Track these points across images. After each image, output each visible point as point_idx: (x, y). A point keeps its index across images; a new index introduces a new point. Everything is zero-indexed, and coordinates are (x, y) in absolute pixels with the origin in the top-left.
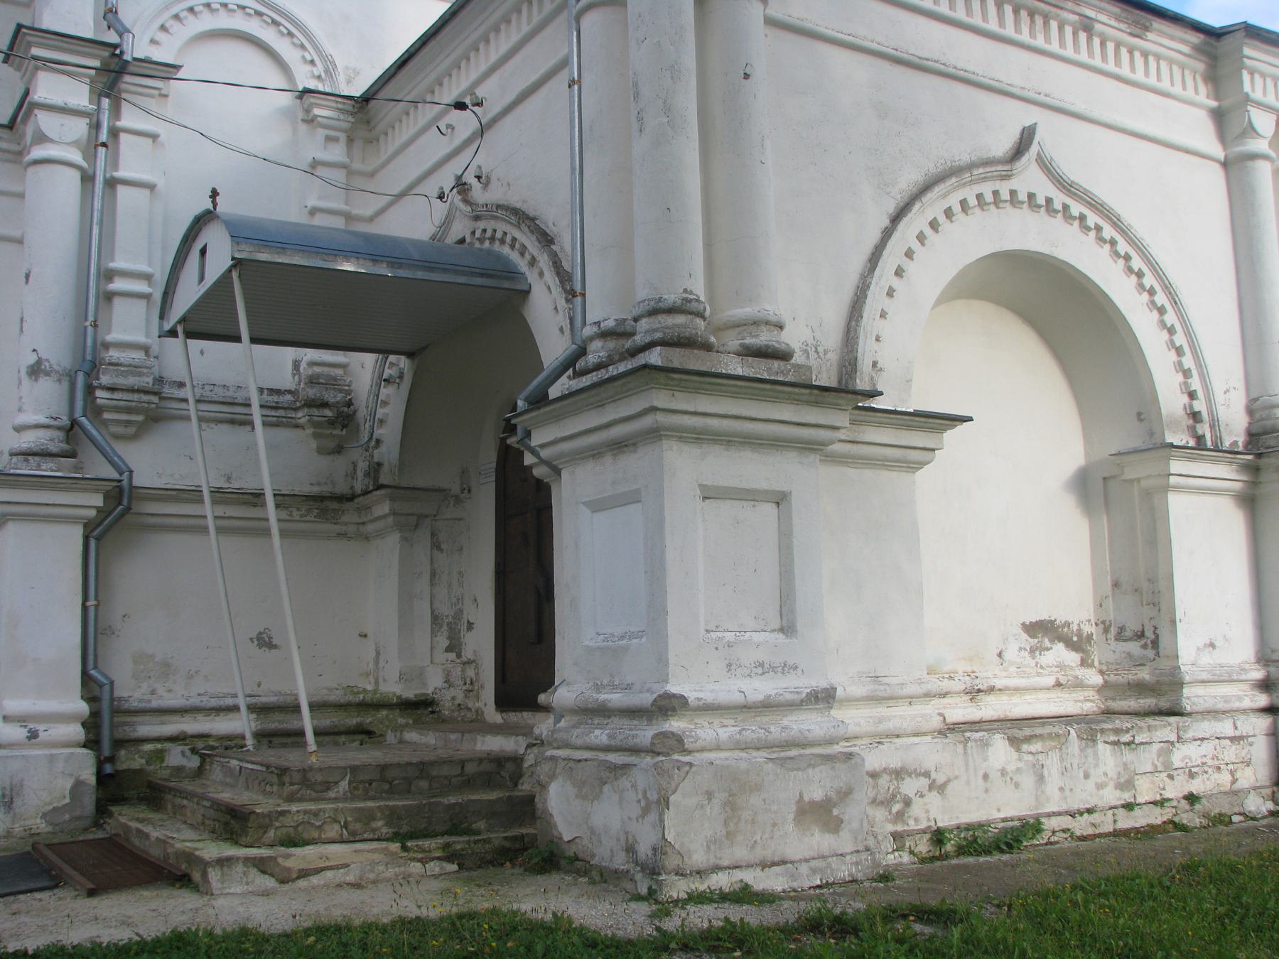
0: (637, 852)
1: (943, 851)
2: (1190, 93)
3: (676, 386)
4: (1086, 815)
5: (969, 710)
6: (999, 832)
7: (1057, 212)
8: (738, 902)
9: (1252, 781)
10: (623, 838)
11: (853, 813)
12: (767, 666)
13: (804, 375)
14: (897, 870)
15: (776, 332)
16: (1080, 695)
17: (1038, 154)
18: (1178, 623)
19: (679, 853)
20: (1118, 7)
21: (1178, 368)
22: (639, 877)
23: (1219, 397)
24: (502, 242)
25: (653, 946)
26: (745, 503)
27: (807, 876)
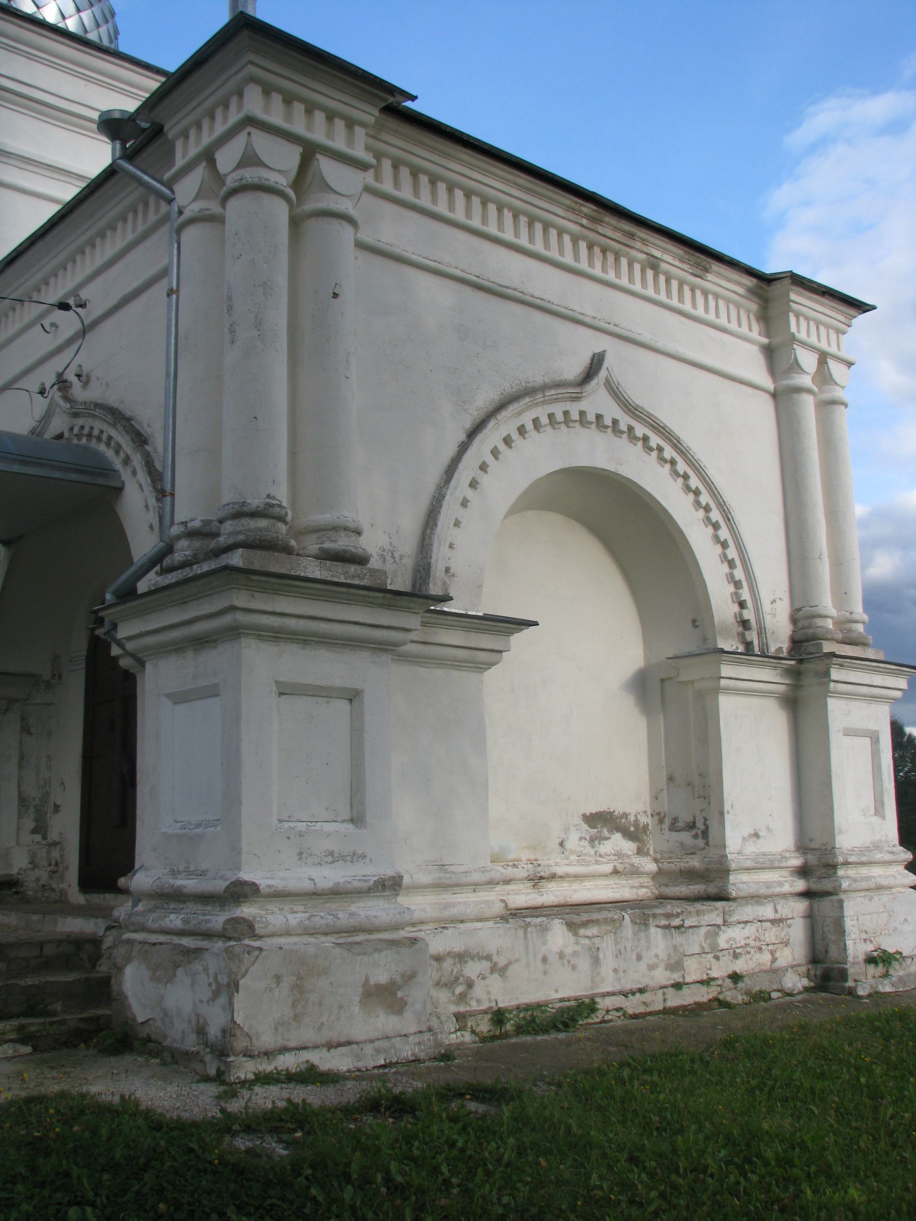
0: (207, 1035)
1: (503, 1030)
2: (744, 329)
3: (255, 587)
4: (638, 995)
5: (532, 896)
6: (557, 1012)
7: (623, 432)
8: (304, 1083)
9: (790, 960)
10: (194, 1021)
11: (415, 995)
12: (336, 855)
13: (379, 579)
14: (459, 1049)
15: (354, 538)
16: (636, 882)
17: (607, 379)
18: (726, 815)
19: (248, 1035)
20: (682, 249)
21: (729, 579)
22: (208, 1058)
23: (767, 607)
24: (99, 439)
25: (217, 1128)
26: (319, 700)
27: (372, 1056)
